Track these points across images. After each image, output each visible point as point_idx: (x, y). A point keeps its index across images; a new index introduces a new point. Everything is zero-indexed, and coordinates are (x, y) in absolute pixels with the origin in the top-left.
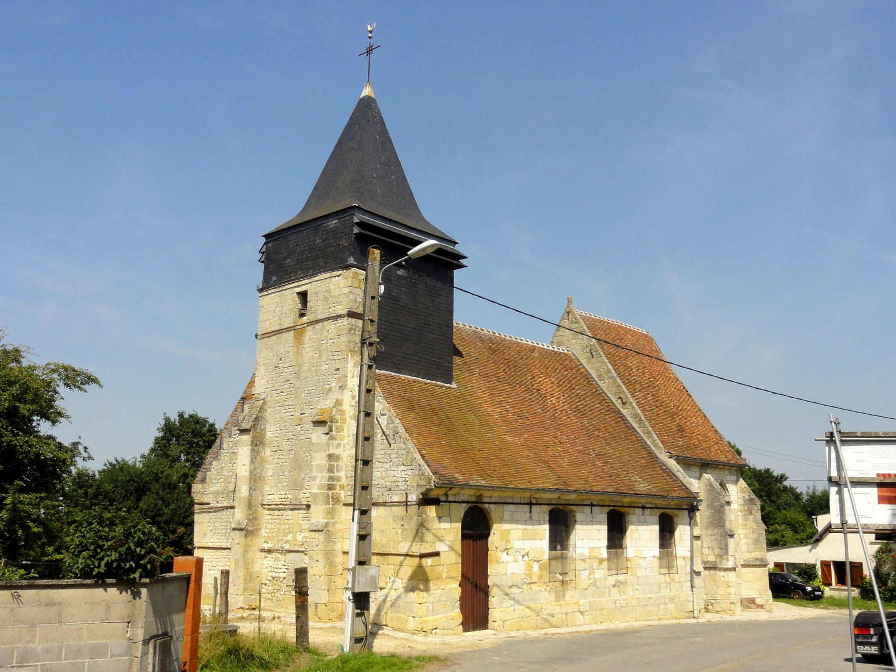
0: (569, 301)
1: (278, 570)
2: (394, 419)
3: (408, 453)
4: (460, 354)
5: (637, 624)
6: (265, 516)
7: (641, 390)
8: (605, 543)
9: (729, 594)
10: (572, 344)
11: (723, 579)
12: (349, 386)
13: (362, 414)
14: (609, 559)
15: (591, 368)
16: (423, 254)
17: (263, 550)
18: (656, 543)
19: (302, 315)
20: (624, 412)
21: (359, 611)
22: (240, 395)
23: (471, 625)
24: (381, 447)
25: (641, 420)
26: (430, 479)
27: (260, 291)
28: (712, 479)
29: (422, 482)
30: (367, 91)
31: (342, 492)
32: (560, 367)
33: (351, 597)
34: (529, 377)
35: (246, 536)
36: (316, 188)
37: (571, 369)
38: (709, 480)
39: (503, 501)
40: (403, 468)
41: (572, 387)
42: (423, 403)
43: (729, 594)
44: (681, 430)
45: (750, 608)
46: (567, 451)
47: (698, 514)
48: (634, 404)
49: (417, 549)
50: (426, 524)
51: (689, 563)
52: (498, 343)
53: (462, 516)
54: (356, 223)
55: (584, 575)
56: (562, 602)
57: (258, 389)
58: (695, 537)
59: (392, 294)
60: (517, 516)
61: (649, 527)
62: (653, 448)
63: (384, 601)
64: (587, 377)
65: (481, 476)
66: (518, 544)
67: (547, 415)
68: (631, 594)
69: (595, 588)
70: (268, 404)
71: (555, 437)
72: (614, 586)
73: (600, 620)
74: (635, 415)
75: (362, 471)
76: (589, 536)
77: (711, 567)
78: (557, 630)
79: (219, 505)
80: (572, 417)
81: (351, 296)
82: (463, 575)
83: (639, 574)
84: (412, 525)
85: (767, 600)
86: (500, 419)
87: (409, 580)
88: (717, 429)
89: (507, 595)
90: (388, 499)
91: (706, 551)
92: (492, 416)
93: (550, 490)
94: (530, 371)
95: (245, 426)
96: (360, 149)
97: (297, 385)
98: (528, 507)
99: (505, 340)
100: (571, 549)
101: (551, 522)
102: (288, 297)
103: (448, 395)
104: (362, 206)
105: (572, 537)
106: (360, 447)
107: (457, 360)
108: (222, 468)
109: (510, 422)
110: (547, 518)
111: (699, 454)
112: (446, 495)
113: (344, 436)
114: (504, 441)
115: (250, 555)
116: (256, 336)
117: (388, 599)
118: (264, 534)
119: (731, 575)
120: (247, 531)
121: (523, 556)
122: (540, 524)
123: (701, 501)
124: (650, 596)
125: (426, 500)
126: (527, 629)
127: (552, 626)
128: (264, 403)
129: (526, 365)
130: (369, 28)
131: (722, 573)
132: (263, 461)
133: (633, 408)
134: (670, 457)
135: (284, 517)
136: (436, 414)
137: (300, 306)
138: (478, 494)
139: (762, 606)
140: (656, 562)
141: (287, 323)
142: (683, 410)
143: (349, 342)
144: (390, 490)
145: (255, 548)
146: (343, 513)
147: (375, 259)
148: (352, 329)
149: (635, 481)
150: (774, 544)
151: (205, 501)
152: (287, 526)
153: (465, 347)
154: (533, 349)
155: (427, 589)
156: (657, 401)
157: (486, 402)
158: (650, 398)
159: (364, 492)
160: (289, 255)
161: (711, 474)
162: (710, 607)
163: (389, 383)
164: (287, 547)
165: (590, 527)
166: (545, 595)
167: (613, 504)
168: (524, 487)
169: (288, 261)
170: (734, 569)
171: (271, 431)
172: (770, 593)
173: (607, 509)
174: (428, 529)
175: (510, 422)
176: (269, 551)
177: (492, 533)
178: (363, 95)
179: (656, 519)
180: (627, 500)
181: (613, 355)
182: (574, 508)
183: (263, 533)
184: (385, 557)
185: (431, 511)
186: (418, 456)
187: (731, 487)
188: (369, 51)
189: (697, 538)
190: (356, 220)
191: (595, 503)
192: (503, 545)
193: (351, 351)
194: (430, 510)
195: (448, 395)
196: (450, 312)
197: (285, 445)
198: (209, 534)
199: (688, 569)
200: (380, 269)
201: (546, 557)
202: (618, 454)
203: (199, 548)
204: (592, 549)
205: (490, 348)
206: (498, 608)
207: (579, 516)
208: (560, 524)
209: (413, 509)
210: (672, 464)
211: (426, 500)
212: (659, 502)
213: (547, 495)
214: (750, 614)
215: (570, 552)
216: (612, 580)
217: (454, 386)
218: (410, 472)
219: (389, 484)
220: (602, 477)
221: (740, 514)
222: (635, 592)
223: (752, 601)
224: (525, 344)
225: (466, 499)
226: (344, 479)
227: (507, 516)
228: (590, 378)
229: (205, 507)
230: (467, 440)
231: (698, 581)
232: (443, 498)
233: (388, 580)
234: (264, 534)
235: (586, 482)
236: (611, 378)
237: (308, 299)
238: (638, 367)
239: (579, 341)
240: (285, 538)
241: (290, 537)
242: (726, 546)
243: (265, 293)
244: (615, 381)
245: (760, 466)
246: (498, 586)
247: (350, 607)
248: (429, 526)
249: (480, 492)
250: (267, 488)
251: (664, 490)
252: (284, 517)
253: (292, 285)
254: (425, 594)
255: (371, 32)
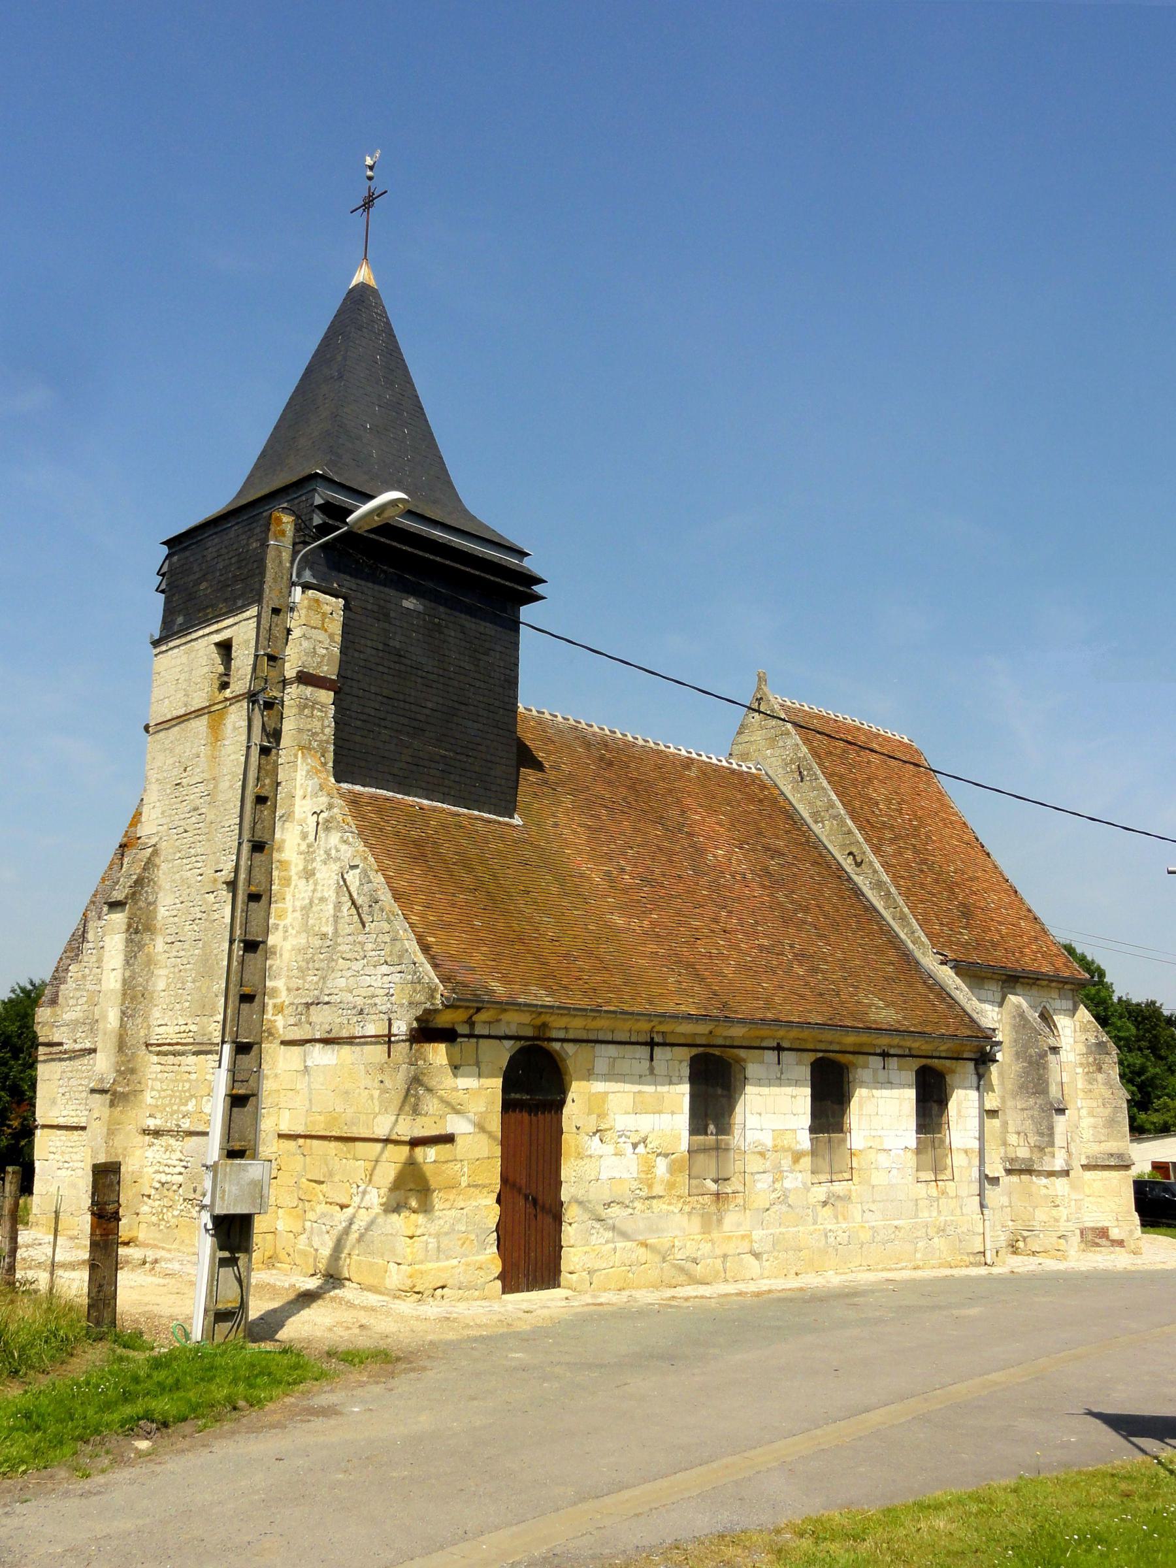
0: (761, 679)
1: (171, 1170)
2: (372, 874)
3: (394, 940)
4: (538, 766)
5: (865, 1278)
6: (152, 1067)
7: (892, 841)
8: (806, 1121)
9: (1057, 1220)
10: (765, 759)
11: (1044, 1191)
12: (297, 816)
13: (246, 847)
14: (814, 1153)
15: (800, 801)
16: (377, 521)
17: (146, 1132)
18: (910, 1121)
19: (224, 686)
20: (858, 879)
21: (226, 1254)
22: (119, 839)
23: (523, 1280)
24: (348, 931)
25: (888, 894)
26: (435, 990)
27: (156, 643)
28: (1025, 1005)
29: (419, 997)
30: (363, 275)
31: (279, 1018)
32: (739, 797)
33: (210, 1226)
34: (674, 812)
35: (112, 1104)
36: (263, 455)
37: (761, 801)
38: (1019, 1006)
39: (592, 1037)
40: (385, 969)
41: (760, 833)
42: (447, 849)
43: (1057, 1220)
44: (967, 912)
45: (1098, 1245)
46: (735, 947)
47: (994, 1068)
48: (877, 865)
49: (408, 1128)
50: (425, 1079)
51: (976, 1162)
52: (619, 750)
53: (505, 1064)
54: (319, 507)
55: (763, 1183)
56: (715, 1235)
57: (146, 829)
58: (988, 1112)
59: (392, 643)
60: (624, 1066)
61: (896, 1093)
62: (911, 946)
63: (347, 1231)
64: (791, 816)
65: (546, 988)
66: (624, 1124)
67: (704, 881)
68: (858, 1218)
69: (784, 1208)
70: (163, 854)
71: (716, 920)
72: (825, 1203)
73: (795, 1269)
74: (879, 885)
75: (242, 963)
76: (773, 1109)
77: (1020, 1169)
78: (703, 1290)
79: (78, 1047)
80: (754, 885)
81: (305, 644)
82: (505, 1180)
83: (874, 1181)
84: (398, 1081)
85: (1131, 1231)
86: (605, 885)
87: (391, 1190)
88: (1038, 915)
89: (600, 1220)
90: (358, 1032)
91: (1013, 1139)
92: (589, 879)
93: (689, 1017)
94: (679, 801)
95: (118, 895)
96: (341, 377)
97: (211, 817)
98: (648, 1048)
99: (634, 745)
100: (737, 1131)
101: (693, 1080)
102: (201, 653)
103: (502, 838)
104: (331, 474)
105: (739, 1109)
106: (238, 913)
107: (529, 775)
108: (84, 977)
109: (625, 891)
110: (686, 1072)
111: (999, 957)
112: (470, 1023)
113: (285, 911)
114: (609, 926)
115: (119, 1141)
116: (147, 728)
117: (355, 1227)
118: (149, 1101)
119: (1060, 1183)
120: (115, 1093)
121: (635, 1146)
122: (671, 1083)
123: (999, 1043)
124: (896, 1223)
125: (426, 1031)
126: (638, 1288)
127: (694, 1280)
128: (155, 853)
129: (670, 791)
130: (369, 161)
131: (1043, 1181)
132: (150, 962)
133: (875, 871)
134: (942, 963)
135: (183, 1069)
136: (470, 870)
137: (221, 669)
138: (538, 1022)
139: (1120, 1243)
140: (911, 1160)
141: (199, 701)
142: (971, 879)
143: (300, 730)
144: (361, 1012)
145: (131, 1128)
146: (281, 1059)
147: (283, 533)
148: (305, 706)
149: (870, 1006)
150: (1138, 1131)
151: (56, 1040)
152: (187, 1085)
153: (549, 753)
154: (688, 763)
155: (425, 1208)
156: (924, 862)
157: (580, 852)
158: (909, 855)
159: (245, 1007)
160: (204, 574)
161: (1023, 995)
162: (1021, 1244)
163: (379, 811)
164: (186, 1125)
165: (775, 1090)
166: (683, 1220)
167: (822, 1046)
168: (636, 1009)
169: (203, 586)
170: (1066, 1173)
171: (166, 905)
172: (1136, 1218)
173: (811, 1057)
174: (429, 1090)
175: (625, 891)
176: (157, 1133)
177: (570, 1096)
178: (354, 283)
179: (911, 1077)
180: (850, 1040)
181: (841, 777)
182: (742, 1053)
183: (148, 1097)
184: (351, 1144)
185: (438, 1053)
186: (413, 946)
187: (1063, 1022)
188: (368, 203)
189: (993, 1113)
190: (318, 501)
191: (785, 1044)
192: (591, 1123)
193: (302, 748)
194: (435, 1051)
195: (502, 838)
196: (512, 683)
197: (189, 931)
198: (61, 1101)
199: (975, 1174)
200: (295, 553)
201: (684, 1146)
202: (839, 955)
203: (44, 1126)
204: (778, 1133)
205: (602, 758)
206: (580, 1245)
207: (752, 1069)
208: (714, 1087)
209: (401, 1050)
210: (947, 975)
211: (426, 1031)
212: (917, 1045)
213: (686, 1028)
214: (1099, 1257)
215: (736, 1139)
216: (820, 1193)
217: (517, 820)
218: (396, 978)
219: (359, 1001)
220: (802, 996)
221: (1079, 1070)
222: (868, 1215)
223: (1103, 1233)
224: (674, 755)
225: (512, 1031)
226: (284, 993)
227: (601, 1065)
228: (796, 818)
229: (55, 1049)
230: (529, 920)
231: (991, 1192)
232: (463, 1029)
233: (354, 1190)
234: (149, 1101)
235: (769, 1004)
236: (835, 817)
237: (234, 655)
238: (889, 801)
239: (778, 752)
240: (183, 1108)
241: (191, 1106)
242: (1051, 1128)
243: (164, 648)
244: (843, 823)
245: (1138, 996)
246: (580, 1203)
247: (206, 1244)
248: (432, 1083)
249: (544, 1018)
250: (156, 1013)
251: (925, 1023)
252: (183, 1069)
253: (207, 630)
254: (420, 1218)
255: (371, 168)
